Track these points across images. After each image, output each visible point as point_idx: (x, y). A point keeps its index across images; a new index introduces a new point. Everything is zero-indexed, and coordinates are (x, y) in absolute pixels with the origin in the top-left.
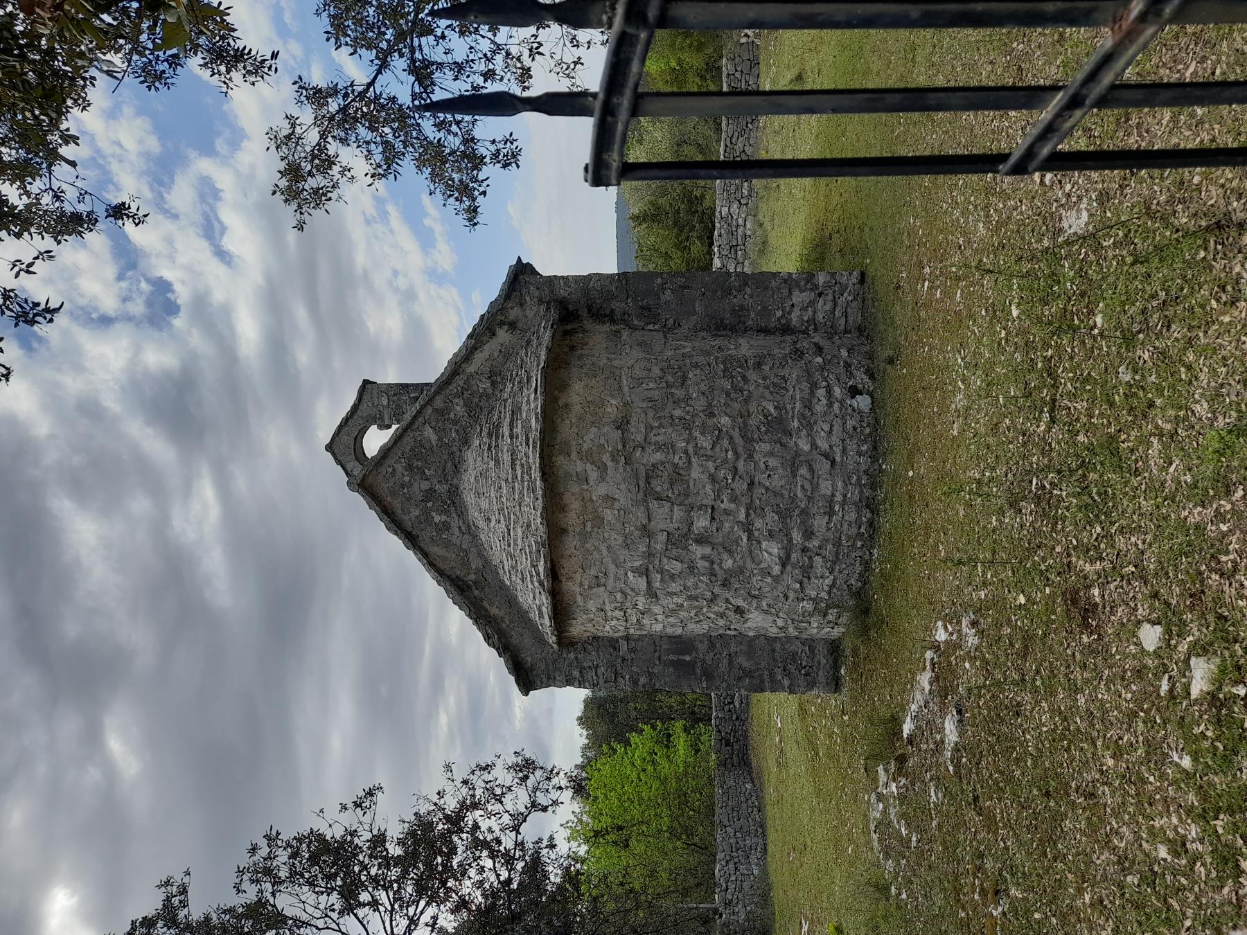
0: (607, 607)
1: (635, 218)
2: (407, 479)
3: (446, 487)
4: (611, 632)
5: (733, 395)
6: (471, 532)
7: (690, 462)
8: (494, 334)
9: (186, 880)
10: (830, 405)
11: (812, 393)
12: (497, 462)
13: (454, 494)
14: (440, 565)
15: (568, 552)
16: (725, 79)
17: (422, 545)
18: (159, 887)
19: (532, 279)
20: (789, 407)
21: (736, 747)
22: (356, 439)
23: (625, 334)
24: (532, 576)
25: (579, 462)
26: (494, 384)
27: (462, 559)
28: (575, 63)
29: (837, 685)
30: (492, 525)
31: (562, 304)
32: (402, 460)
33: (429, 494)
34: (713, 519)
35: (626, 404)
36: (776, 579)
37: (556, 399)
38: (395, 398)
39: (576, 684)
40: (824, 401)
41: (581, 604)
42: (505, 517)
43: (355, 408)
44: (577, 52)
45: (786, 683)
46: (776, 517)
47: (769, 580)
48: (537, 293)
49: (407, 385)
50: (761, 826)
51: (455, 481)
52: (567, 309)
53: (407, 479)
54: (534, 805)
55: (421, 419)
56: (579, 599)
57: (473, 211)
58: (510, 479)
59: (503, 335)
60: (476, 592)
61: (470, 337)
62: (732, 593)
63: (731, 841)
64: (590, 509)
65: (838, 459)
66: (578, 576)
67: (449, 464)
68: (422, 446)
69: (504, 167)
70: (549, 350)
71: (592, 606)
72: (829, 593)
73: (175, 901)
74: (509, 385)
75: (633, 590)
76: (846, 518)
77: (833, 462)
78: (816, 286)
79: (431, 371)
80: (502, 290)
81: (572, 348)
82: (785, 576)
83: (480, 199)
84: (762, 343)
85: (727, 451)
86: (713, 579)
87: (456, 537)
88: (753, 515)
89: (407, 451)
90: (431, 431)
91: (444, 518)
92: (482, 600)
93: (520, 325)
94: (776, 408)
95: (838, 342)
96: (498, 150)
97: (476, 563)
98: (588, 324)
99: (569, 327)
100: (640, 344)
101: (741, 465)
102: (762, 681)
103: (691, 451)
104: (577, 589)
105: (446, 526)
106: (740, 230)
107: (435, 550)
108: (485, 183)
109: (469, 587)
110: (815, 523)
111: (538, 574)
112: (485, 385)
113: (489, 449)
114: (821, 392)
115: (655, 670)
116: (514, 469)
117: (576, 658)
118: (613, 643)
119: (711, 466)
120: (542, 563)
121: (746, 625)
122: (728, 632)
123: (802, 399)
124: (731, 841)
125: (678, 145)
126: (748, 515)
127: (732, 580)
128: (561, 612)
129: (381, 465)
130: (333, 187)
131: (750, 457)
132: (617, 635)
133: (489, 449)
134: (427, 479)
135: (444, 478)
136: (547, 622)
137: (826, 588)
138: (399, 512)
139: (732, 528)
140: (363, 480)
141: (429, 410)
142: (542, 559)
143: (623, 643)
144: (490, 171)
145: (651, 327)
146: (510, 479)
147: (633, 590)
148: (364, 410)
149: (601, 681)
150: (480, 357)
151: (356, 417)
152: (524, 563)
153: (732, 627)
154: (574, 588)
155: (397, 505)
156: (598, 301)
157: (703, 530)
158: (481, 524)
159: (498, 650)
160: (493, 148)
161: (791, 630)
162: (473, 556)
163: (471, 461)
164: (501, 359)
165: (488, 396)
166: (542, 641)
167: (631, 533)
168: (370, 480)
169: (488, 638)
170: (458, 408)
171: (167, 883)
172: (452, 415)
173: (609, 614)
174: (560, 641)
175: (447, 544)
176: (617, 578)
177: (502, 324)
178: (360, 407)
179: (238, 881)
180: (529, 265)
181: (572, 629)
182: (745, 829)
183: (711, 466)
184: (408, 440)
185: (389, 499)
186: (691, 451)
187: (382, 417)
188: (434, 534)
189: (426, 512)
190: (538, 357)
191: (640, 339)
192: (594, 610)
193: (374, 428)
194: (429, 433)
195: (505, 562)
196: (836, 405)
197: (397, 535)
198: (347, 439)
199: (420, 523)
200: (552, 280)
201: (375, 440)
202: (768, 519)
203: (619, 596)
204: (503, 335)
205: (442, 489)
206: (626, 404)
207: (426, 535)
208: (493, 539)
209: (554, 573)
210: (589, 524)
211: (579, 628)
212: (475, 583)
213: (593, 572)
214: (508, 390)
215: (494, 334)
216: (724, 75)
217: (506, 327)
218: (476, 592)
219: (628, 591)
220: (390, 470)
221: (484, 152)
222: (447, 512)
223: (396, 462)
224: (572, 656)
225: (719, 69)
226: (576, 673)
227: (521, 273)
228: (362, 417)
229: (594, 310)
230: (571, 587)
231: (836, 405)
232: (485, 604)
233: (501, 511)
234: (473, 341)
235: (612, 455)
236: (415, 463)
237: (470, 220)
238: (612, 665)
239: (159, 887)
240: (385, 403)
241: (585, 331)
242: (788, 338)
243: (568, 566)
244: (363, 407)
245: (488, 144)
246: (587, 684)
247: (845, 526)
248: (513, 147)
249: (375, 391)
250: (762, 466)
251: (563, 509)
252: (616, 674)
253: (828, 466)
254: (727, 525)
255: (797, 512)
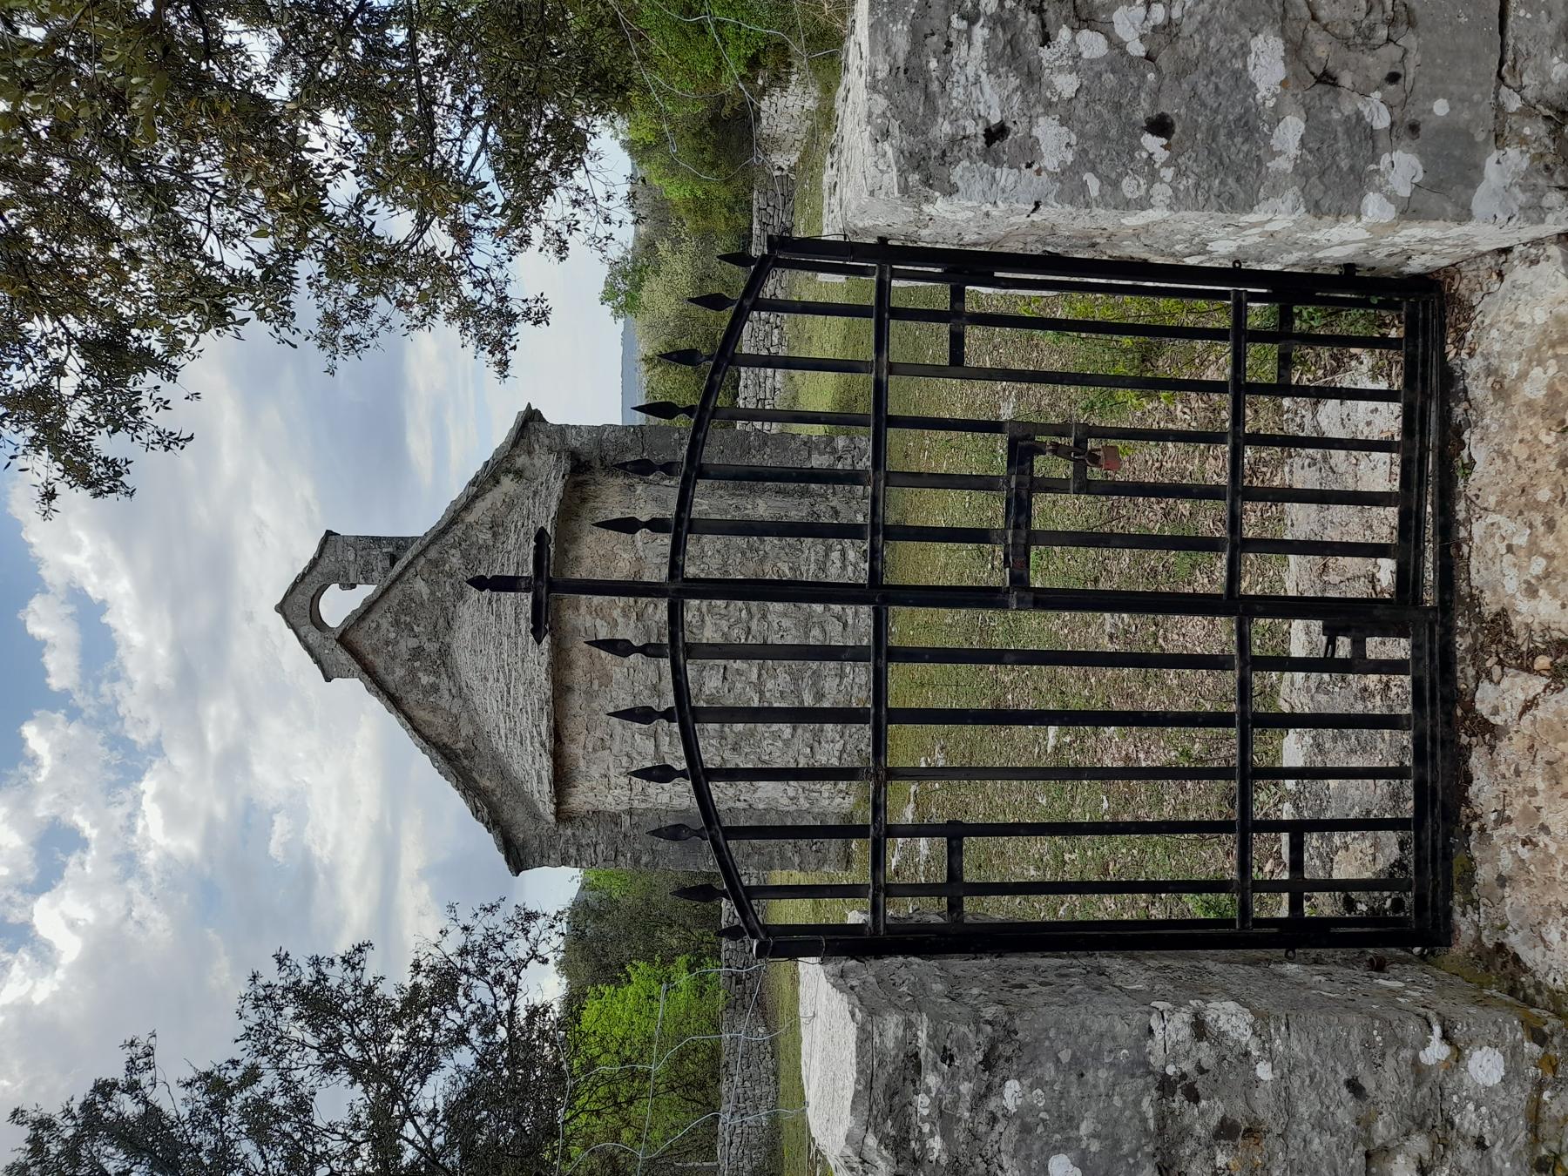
0: (612, 773)
1: (647, 360)
2: (392, 635)
3: (437, 646)
4: (613, 803)
5: (749, 554)
6: (460, 694)
7: (703, 621)
8: (498, 482)
9: (152, 1042)
10: (844, 568)
11: (827, 555)
12: (498, 616)
13: (445, 652)
14: (427, 731)
15: (573, 712)
16: (755, 214)
17: (406, 708)
18: (123, 1047)
19: (542, 425)
20: (804, 569)
21: (749, 984)
22: (312, 599)
23: (640, 489)
24: (532, 737)
25: (588, 617)
26: (495, 535)
27: (451, 725)
28: (607, 238)
29: (848, 862)
30: (489, 684)
31: (574, 455)
32: (389, 615)
33: (417, 653)
34: (725, 678)
35: (639, 559)
36: (787, 743)
37: (566, 552)
38: (364, 553)
39: (572, 863)
40: (838, 564)
41: (584, 769)
42: (504, 673)
43: (314, 563)
44: (609, 229)
45: (797, 860)
46: (788, 678)
47: (780, 744)
48: (547, 442)
49: (379, 539)
50: (774, 1074)
51: (447, 639)
52: (579, 460)
53: (392, 635)
54: (534, 955)
55: (412, 570)
56: (582, 763)
57: (504, 365)
58: (513, 634)
59: (508, 484)
60: (466, 762)
61: (472, 483)
62: (742, 758)
63: (739, 1091)
64: (598, 666)
65: (850, 621)
66: (582, 738)
67: (441, 621)
68: (412, 600)
69: (535, 324)
70: (561, 501)
71: (595, 772)
72: (840, 759)
73: (140, 1063)
74: (513, 537)
75: (640, 753)
76: (857, 680)
77: (845, 625)
78: (835, 450)
79: (418, 522)
80: (509, 436)
81: (584, 500)
82: (796, 740)
83: (511, 353)
84: (781, 504)
85: (741, 611)
86: (723, 742)
87: (446, 701)
88: (765, 676)
89: (394, 604)
90: (423, 583)
91: (432, 679)
92: (471, 770)
93: (527, 474)
94: (790, 568)
95: (855, 507)
96: (529, 309)
97: (466, 730)
98: (599, 477)
99: (580, 478)
100: (655, 500)
101: (754, 625)
102: (772, 858)
103: (704, 609)
104: (580, 752)
105: (435, 689)
106: (769, 382)
107: (421, 715)
108: (515, 338)
109: (457, 756)
110: (827, 685)
111: (540, 734)
112: (485, 536)
113: (490, 603)
114: (835, 555)
115: (659, 848)
116: (517, 622)
117: (574, 834)
118: (615, 818)
119: (724, 624)
120: (545, 722)
121: (756, 796)
122: (738, 805)
123: (817, 561)
124: (739, 1091)
125: (701, 280)
126: (760, 676)
127: (743, 744)
128: (562, 779)
129: (364, 619)
130: (373, 336)
131: (764, 617)
132: (619, 808)
133: (490, 603)
134: (415, 636)
135: (434, 635)
136: (546, 787)
137: (837, 754)
138: (381, 671)
139: (744, 689)
140: (341, 635)
141: (422, 561)
142: (545, 718)
143: (626, 818)
144: (523, 329)
145: (666, 482)
146: (513, 634)
147: (640, 753)
148: (327, 564)
149: (600, 860)
150: (481, 506)
151: (314, 573)
152: (525, 723)
153: (742, 798)
154: (576, 751)
155: (379, 663)
156: (612, 453)
157: (714, 691)
158: (476, 684)
159: (487, 825)
160: (524, 307)
161: (802, 800)
162: (463, 721)
163: (467, 616)
164: (503, 509)
165: (487, 547)
166: (536, 817)
167: (640, 692)
168: (351, 636)
169: (476, 812)
170: (454, 560)
171: (132, 1044)
172: (447, 567)
173: (613, 780)
174: (558, 813)
175: (435, 709)
176: (623, 741)
177: (508, 471)
178: (321, 562)
179: (239, 1007)
180: (537, 412)
181: (571, 800)
182: (755, 1077)
183: (724, 624)
184: (396, 593)
185: (371, 657)
186: (704, 609)
187: (346, 574)
188: (421, 696)
189: (412, 672)
190: (548, 508)
191: (655, 494)
192: (597, 776)
193: (335, 587)
194: (420, 586)
195: (502, 725)
196: (850, 568)
197: (378, 695)
198: (302, 599)
199: (404, 684)
200: (562, 429)
201: (337, 605)
202: (780, 680)
203: (625, 760)
204: (508, 484)
205: (432, 647)
206: (639, 559)
207: (412, 698)
208: (489, 703)
209: (558, 734)
210: (596, 682)
211: (580, 799)
212: (464, 751)
213: (598, 734)
214: (512, 540)
215: (498, 482)
216: (755, 208)
217: (511, 476)
218: (466, 762)
219: (635, 755)
220: (374, 625)
221: (516, 310)
222: (437, 674)
223: (382, 616)
224: (569, 832)
225: (749, 203)
226: (572, 851)
227: (530, 420)
228: (322, 574)
229: (608, 462)
230: (575, 750)
231: (850, 568)
232: (475, 775)
233: (500, 668)
234: (475, 489)
235: (623, 610)
236: (403, 618)
237: (501, 373)
238: (612, 842)
239: (123, 1047)
240: (352, 558)
241: (596, 483)
242: (806, 501)
243: (575, 726)
244: (324, 562)
245: (520, 303)
246: (584, 864)
247: (856, 689)
248: (544, 306)
249: (340, 544)
250: (776, 627)
251: (569, 666)
252: (616, 852)
253: (840, 629)
254: (739, 685)
255: (809, 673)
